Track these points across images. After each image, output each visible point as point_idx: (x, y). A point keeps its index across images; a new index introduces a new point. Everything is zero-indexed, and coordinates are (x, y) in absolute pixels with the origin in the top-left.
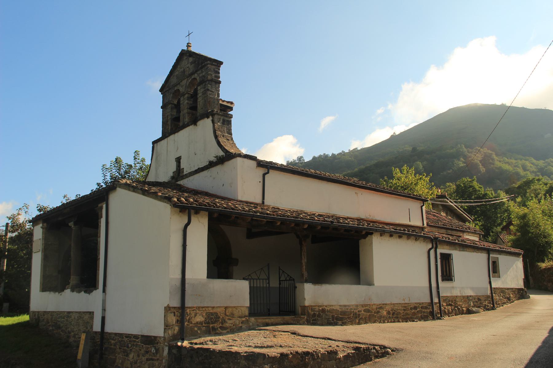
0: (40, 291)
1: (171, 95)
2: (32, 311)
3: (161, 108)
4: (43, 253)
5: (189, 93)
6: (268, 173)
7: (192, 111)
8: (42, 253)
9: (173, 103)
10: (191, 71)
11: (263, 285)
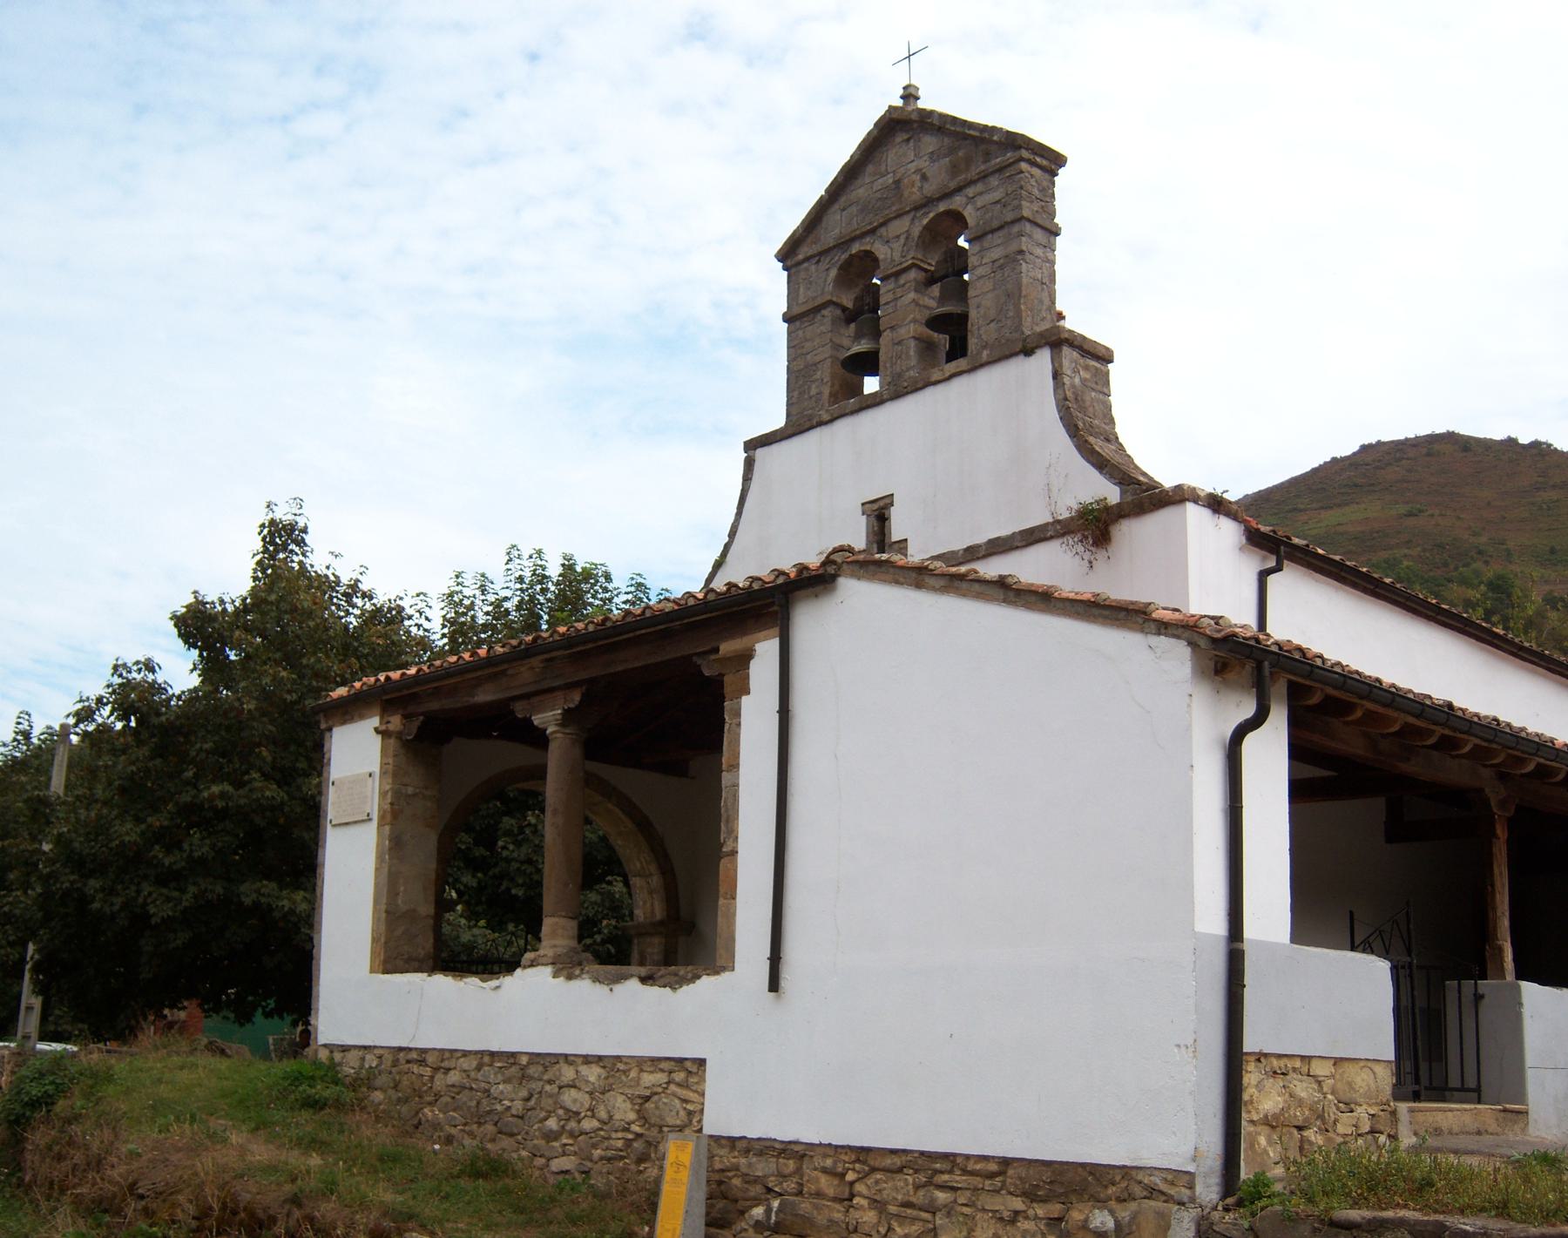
0: (372, 971)
1: (833, 273)
2: (325, 1046)
3: (784, 321)
4: (387, 828)
5: (922, 265)
6: (1278, 569)
7: (931, 332)
8: (380, 825)
9: (839, 301)
10: (930, 189)
11: (1476, 984)
